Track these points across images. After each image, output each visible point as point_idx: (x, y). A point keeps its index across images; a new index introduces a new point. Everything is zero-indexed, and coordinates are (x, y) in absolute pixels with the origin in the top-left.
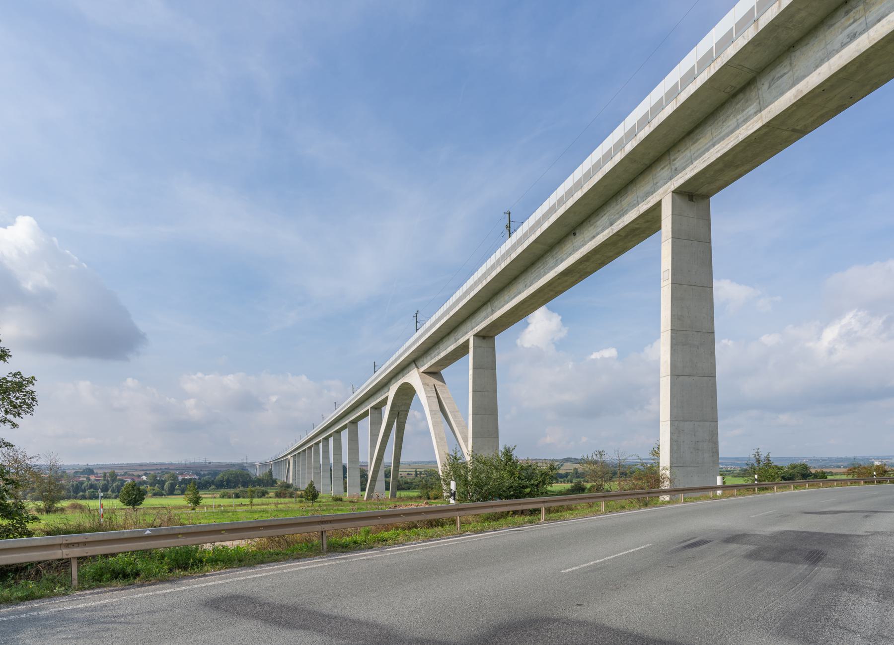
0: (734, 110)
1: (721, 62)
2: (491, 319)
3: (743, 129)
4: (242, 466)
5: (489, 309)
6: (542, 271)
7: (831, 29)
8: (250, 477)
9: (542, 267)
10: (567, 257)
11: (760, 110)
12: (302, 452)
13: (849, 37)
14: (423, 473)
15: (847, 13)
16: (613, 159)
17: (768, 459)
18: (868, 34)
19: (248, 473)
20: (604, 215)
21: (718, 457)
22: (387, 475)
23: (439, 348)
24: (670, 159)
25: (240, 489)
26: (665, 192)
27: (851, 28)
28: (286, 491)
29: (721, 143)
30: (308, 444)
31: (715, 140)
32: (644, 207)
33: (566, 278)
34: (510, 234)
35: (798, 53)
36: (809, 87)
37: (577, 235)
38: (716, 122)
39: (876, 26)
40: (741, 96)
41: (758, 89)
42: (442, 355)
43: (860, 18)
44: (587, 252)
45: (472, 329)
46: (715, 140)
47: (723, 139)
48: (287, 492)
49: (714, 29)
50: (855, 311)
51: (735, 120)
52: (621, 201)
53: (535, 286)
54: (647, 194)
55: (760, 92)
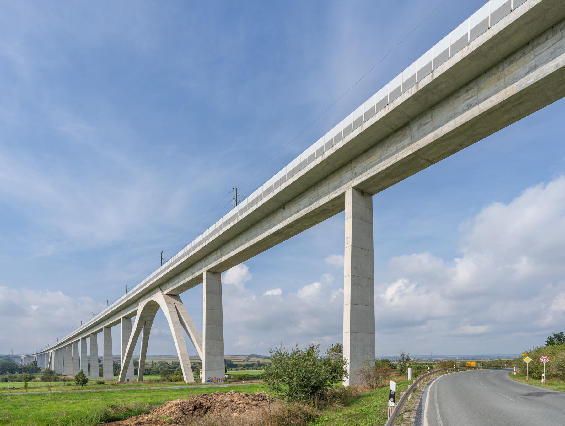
0: (395, 140)
1: (393, 106)
2: (220, 261)
3: (400, 153)
4: (8, 357)
5: (219, 254)
6: (259, 231)
7: (458, 99)
8: (17, 366)
9: (260, 228)
10: (278, 223)
11: (412, 143)
12: (61, 349)
13: (468, 106)
14: (157, 363)
15: (467, 91)
16: (316, 160)
17: (408, 356)
18: (479, 107)
19: (14, 362)
20: (305, 198)
21: (375, 356)
22: (136, 364)
23: (179, 278)
24: (352, 166)
25: (7, 375)
26: (348, 187)
27: (469, 101)
28: (49, 376)
29: (386, 160)
30: (68, 342)
31: (382, 158)
32: (333, 196)
33: (276, 237)
34: (236, 203)
35: (436, 111)
36: (442, 133)
37: (286, 209)
38: (383, 146)
39: (483, 102)
40: (400, 132)
41: (411, 130)
42: (182, 283)
43: (474, 96)
44: (293, 221)
45: (205, 266)
46: (382, 158)
47: (387, 158)
48: (52, 377)
49: (388, 84)
50: (403, 279)
51: (396, 147)
52: (317, 189)
53: (254, 240)
54: (335, 187)
55: (412, 131)
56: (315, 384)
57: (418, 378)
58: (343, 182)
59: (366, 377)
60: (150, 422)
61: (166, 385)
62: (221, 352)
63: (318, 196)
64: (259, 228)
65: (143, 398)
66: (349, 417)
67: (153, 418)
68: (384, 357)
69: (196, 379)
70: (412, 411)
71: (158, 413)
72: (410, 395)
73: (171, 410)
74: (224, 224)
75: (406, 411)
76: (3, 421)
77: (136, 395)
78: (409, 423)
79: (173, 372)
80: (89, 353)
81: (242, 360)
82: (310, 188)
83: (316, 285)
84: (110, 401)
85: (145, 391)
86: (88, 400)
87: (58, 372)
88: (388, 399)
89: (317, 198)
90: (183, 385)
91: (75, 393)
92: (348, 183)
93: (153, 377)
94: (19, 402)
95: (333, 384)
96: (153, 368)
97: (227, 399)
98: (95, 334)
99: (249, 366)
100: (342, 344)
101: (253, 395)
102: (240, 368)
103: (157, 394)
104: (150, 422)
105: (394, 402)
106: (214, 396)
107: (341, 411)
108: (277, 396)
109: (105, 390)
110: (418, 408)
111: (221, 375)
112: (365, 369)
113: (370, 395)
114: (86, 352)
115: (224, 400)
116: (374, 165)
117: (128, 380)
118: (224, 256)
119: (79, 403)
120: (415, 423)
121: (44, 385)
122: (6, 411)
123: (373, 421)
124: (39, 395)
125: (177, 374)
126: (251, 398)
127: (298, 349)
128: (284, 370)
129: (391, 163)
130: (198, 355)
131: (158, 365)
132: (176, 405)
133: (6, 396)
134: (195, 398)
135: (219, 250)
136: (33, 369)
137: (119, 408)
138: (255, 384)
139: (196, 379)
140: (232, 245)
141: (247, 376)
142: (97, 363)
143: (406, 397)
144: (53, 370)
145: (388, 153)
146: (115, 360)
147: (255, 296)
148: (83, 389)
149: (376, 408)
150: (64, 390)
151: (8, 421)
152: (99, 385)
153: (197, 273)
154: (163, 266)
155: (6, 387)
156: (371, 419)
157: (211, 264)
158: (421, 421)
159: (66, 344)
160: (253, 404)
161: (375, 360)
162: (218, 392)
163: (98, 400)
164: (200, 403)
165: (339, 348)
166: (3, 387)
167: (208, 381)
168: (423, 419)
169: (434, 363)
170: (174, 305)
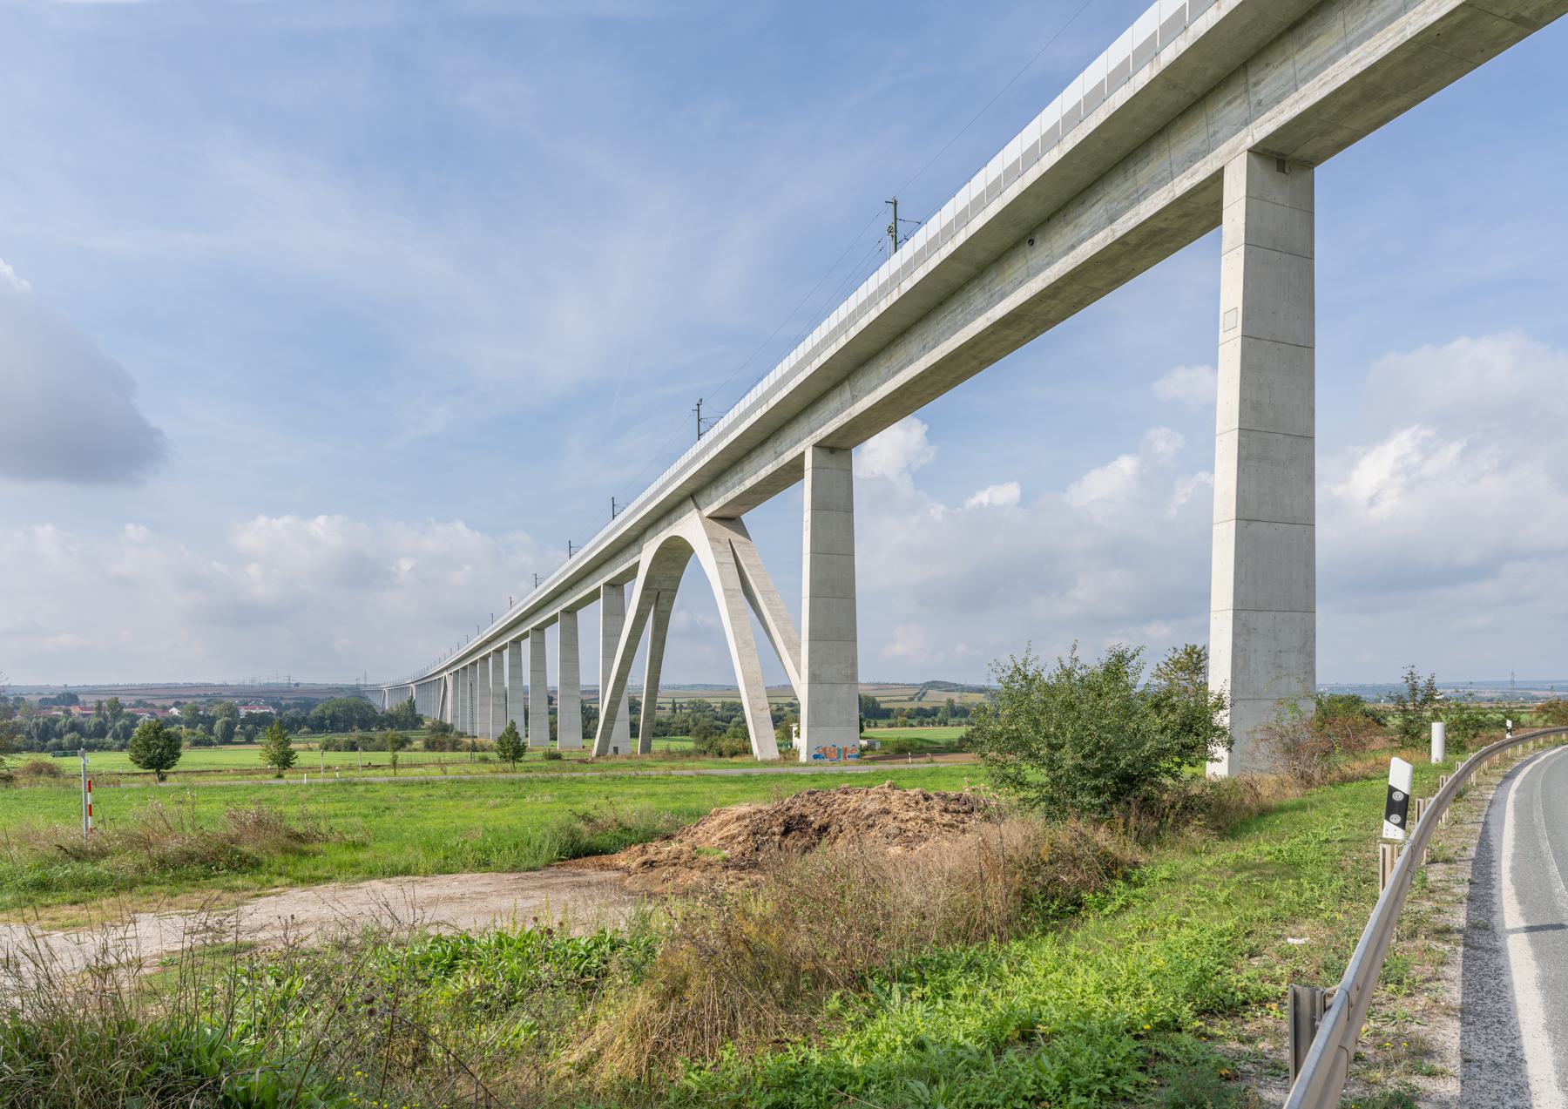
2: (850, 414)
4: (357, 691)
8: (374, 711)
12: (467, 668)
14: (685, 705)
20: (1097, 202)
21: (1314, 682)
22: (634, 707)
23: (742, 470)
28: (443, 738)
29: (1365, 44)
31: (1351, 38)
32: (1183, 184)
33: (1007, 332)
34: (896, 244)
37: (1037, 243)
42: (749, 483)
47: (1368, 35)
48: (446, 740)
56: (1130, 766)
57: (1472, 756)
58: (1218, 135)
59: (1288, 751)
60: (676, 861)
61: (707, 765)
62: (849, 672)
63: (1137, 191)
64: (957, 308)
65: (654, 798)
66: (1237, 871)
67: (681, 852)
68: (1343, 689)
69: (783, 749)
70: (1455, 862)
71: (694, 839)
72: (1445, 810)
73: (725, 832)
74: (862, 309)
75: (1434, 861)
76: (354, 842)
77: (637, 789)
78: (1450, 898)
79: (725, 731)
80: (527, 681)
81: (906, 698)
82: (1111, 170)
83: (1127, 464)
84: (577, 803)
85: (657, 781)
86: (528, 799)
87: (458, 728)
88: (1383, 814)
89: (1132, 198)
90: (751, 765)
91: (498, 781)
92: (1234, 138)
93: (677, 744)
94: (382, 800)
95: (1183, 768)
96: (675, 719)
97: (872, 807)
98: (540, 629)
99: (924, 716)
100: (1204, 648)
101: (944, 797)
102: (900, 719)
103: (687, 788)
104: (676, 861)
105: (1404, 828)
106: (838, 795)
107: (1209, 853)
108: (1014, 799)
109: (565, 775)
110: (1477, 853)
111: (852, 739)
112: (1285, 724)
113: (1302, 807)
114: (521, 677)
115: (865, 807)
116: (1324, 67)
117: (616, 749)
118: (861, 399)
119: (507, 806)
120: (1470, 899)
121: (432, 761)
122: (358, 820)
123: (1322, 886)
124: (421, 784)
125: (735, 736)
126: (938, 804)
127: (1076, 660)
128: (1036, 723)
129: (1384, 50)
130: (787, 683)
131: (688, 711)
132: (738, 819)
133: (355, 784)
134: (788, 800)
135: (847, 383)
136: (406, 720)
137: (600, 821)
138: (942, 766)
139: (783, 749)
140: (882, 366)
141: (919, 743)
142: (544, 705)
143: (1435, 814)
144: (449, 722)
145: (1373, 18)
146: (585, 697)
147: (942, 508)
148: (514, 772)
149: (1327, 847)
150: (474, 772)
151: (364, 845)
152: (549, 762)
153: (789, 453)
154: (702, 439)
155: (353, 762)
156: (1314, 879)
157: (824, 424)
158: (1492, 896)
159: (477, 657)
160: (944, 822)
161: (1311, 694)
162: (846, 785)
163: (547, 798)
164: (801, 816)
165: (1194, 660)
166: (348, 762)
167: (816, 757)
168: (1500, 890)
169: (1522, 707)
170: (729, 546)
